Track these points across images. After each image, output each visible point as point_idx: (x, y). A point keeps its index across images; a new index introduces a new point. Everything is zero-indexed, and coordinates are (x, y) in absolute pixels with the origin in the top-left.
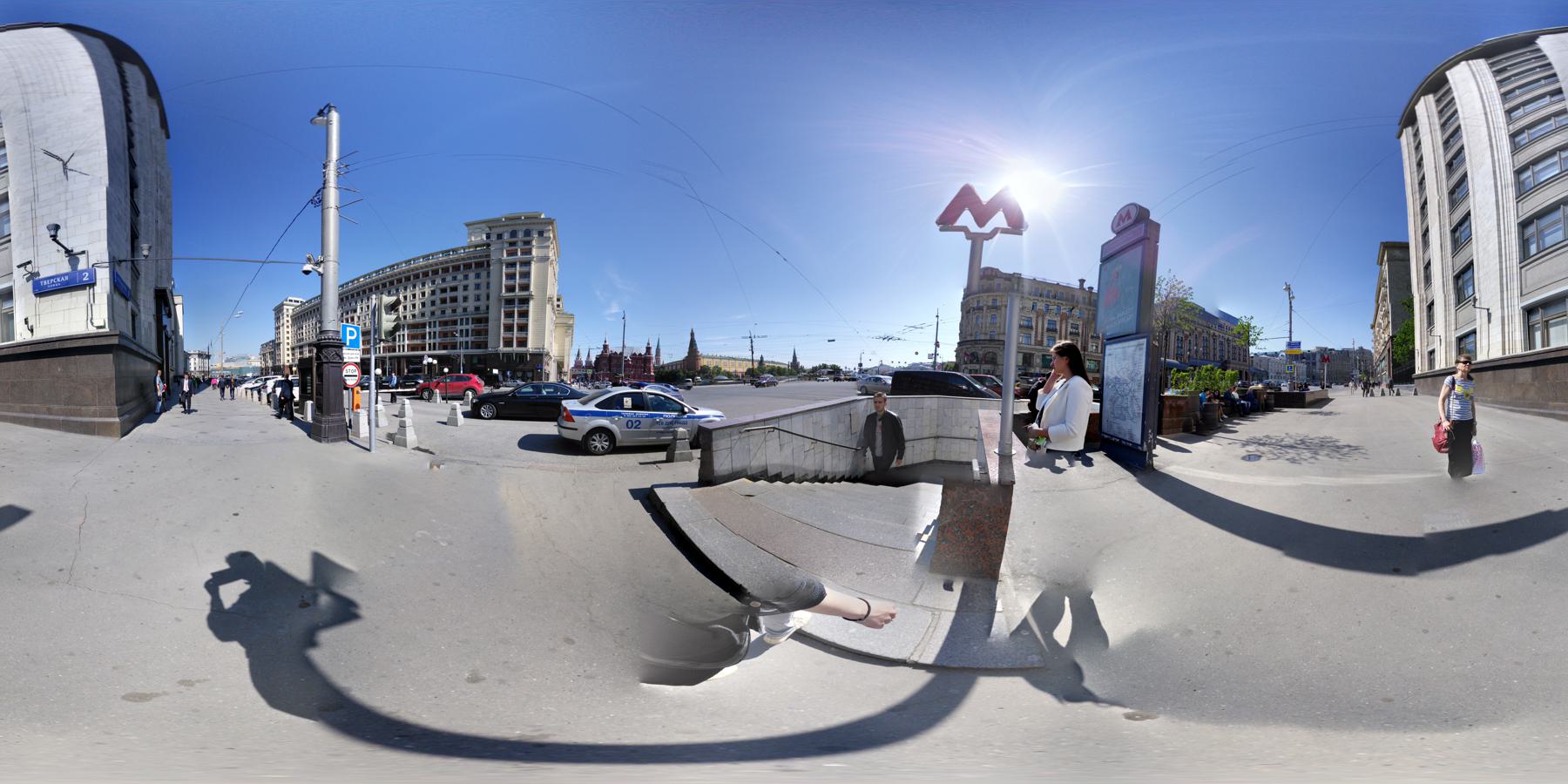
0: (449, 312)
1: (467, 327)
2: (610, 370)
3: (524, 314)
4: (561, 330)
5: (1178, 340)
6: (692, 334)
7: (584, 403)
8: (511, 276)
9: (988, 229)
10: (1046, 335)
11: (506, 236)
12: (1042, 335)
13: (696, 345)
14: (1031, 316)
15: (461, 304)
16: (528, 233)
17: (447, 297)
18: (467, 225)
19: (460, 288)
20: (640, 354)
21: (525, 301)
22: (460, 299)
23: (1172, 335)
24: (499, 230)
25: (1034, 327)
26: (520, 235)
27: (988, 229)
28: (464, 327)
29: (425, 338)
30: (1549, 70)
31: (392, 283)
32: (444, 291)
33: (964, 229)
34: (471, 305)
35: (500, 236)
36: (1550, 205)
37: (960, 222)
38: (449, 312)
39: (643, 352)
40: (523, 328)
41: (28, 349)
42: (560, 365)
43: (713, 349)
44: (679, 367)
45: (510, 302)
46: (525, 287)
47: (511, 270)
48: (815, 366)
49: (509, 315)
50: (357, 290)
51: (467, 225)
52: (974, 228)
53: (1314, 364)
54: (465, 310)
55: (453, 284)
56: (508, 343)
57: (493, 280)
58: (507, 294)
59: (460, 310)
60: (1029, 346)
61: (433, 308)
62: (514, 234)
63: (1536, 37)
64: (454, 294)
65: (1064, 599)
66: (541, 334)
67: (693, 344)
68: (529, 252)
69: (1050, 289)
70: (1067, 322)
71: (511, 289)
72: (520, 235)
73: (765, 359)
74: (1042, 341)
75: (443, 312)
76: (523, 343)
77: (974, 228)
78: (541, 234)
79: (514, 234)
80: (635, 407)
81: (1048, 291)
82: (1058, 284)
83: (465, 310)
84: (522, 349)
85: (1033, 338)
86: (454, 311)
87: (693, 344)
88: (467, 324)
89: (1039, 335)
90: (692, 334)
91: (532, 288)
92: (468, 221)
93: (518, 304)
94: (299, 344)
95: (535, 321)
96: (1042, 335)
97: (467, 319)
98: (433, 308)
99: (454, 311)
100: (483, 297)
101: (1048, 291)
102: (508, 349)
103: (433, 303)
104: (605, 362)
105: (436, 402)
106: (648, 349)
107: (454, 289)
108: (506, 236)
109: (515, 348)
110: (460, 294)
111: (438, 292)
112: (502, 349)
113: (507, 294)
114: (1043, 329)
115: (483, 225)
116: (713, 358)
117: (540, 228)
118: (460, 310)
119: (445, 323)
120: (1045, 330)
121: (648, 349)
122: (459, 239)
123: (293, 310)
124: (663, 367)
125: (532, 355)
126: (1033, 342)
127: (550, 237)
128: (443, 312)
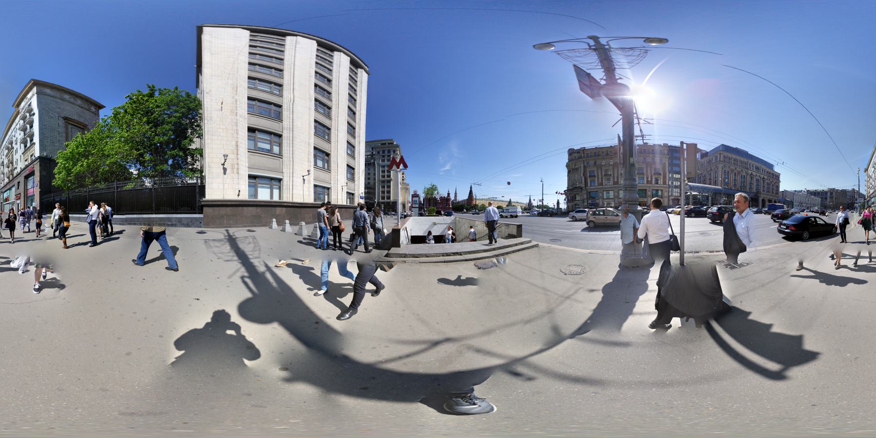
3: (389, 187)
4: (404, 191)
5: (725, 172)
6: (471, 188)
7: (673, 211)
8: (383, 172)
10: (604, 178)
11: (381, 153)
12: (602, 178)
13: (472, 193)
14: (594, 169)
20: (444, 197)
21: (389, 181)
23: (720, 169)
24: (378, 150)
25: (596, 175)
26: (386, 152)
30: (269, 117)
35: (379, 153)
39: (446, 196)
40: (389, 192)
41: (290, 205)
42: (404, 206)
43: (481, 195)
44: (466, 202)
45: (383, 182)
47: (383, 169)
49: (383, 187)
53: (826, 198)
58: (383, 179)
60: (642, 185)
62: (384, 152)
63: (362, 68)
65: (779, 362)
66: (396, 194)
67: (471, 192)
69: (595, 151)
70: (601, 169)
71: (383, 177)
72: (386, 152)
73: (512, 201)
74: (602, 182)
76: (389, 198)
78: (394, 152)
79: (384, 152)
80: (604, 215)
81: (594, 153)
82: (596, 148)
84: (388, 200)
85: (645, 179)
87: (471, 192)
89: (600, 180)
90: (471, 188)
91: (392, 177)
95: (393, 189)
96: (602, 178)
100: (372, 179)
101: (594, 153)
105: (271, 228)
106: (449, 194)
108: (381, 153)
109: (386, 200)
113: (383, 179)
114: (602, 175)
116: (482, 200)
117: (394, 149)
120: (603, 176)
121: (449, 194)
124: (458, 202)
125: (393, 202)
126: (596, 185)
127: (397, 154)
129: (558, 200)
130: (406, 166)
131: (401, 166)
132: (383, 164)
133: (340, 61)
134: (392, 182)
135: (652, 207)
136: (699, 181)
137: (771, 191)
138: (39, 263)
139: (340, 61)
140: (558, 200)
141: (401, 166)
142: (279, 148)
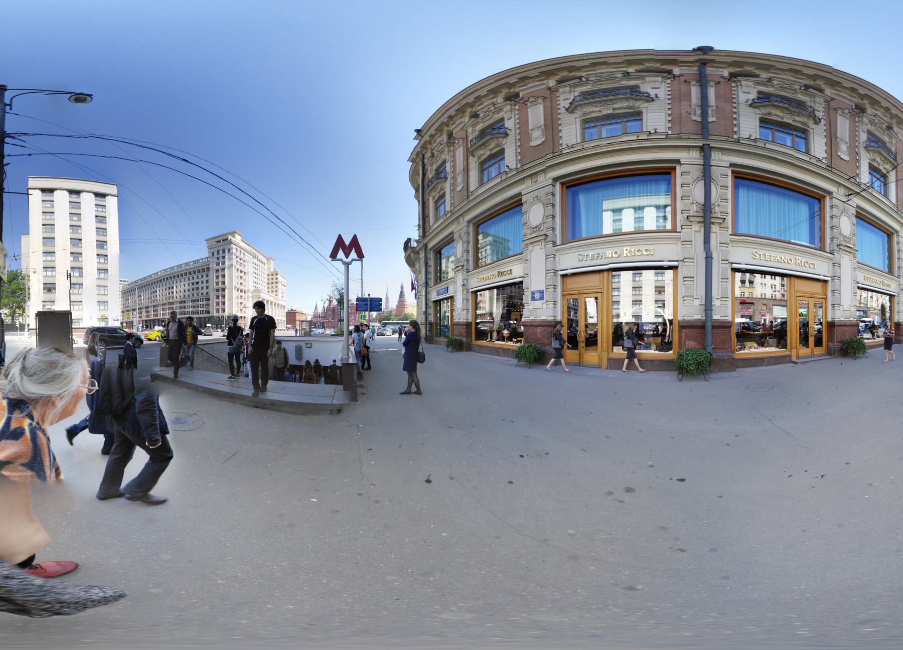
0: (195, 295)
1: (203, 303)
2: (334, 319)
6: (402, 287)
9: (349, 260)
11: (216, 254)
15: (201, 291)
16: (224, 251)
17: (195, 286)
18: (206, 240)
19: (200, 283)
21: (224, 290)
22: (200, 288)
26: (221, 252)
27: (349, 260)
28: (202, 303)
29: (219, 298)
31: (178, 276)
32: (193, 284)
33: (341, 260)
34: (205, 291)
36: (706, 59)
37: (338, 257)
38: (195, 295)
40: (224, 303)
45: (218, 290)
46: (223, 283)
48: (403, 247)
49: (218, 297)
50: (170, 276)
51: (206, 240)
52: (345, 259)
54: (202, 294)
55: (197, 280)
56: (218, 311)
57: (210, 278)
59: (200, 294)
61: (189, 293)
62: (218, 253)
64: (197, 286)
66: (231, 307)
68: (224, 263)
72: (221, 252)
75: (193, 295)
76: (224, 311)
77: (345, 259)
78: (229, 250)
79: (218, 253)
83: (202, 294)
86: (198, 295)
88: (203, 301)
90: (402, 287)
92: (207, 238)
93: (221, 291)
94: (153, 304)
97: (203, 299)
98: (189, 293)
99: (198, 295)
102: (217, 314)
103: (189, 290)
104: (330, 313)
107: (197, 283)
108: (216, 254)
109: (221, 314)
110: (200, 286)
111: (191, 284)
112: (215, 314)
115: (212, 241)
118: (200, 294)
119: (194, 301)
122: (702, 145)
123: (123, 287)
128: (193, 295)
129: (677, 480)
130: (361, 256)
131: (353, 255)
132: (218, 267)
133: (152, 207)
134: (226, 290)
135: (637, 225)
136: (366, 366)
137: (144, 311)
138: (368, 371)
139: (152, 207)
140: (677, 480)
141: (353, 255)
142: (442, 249)
